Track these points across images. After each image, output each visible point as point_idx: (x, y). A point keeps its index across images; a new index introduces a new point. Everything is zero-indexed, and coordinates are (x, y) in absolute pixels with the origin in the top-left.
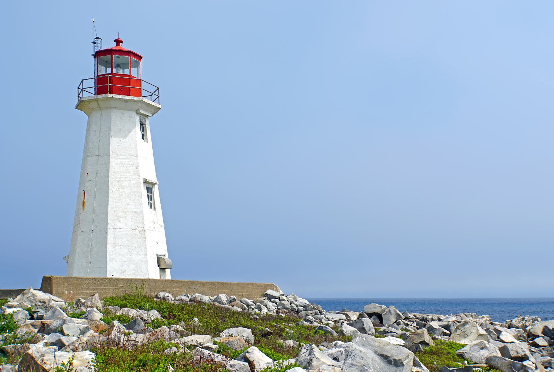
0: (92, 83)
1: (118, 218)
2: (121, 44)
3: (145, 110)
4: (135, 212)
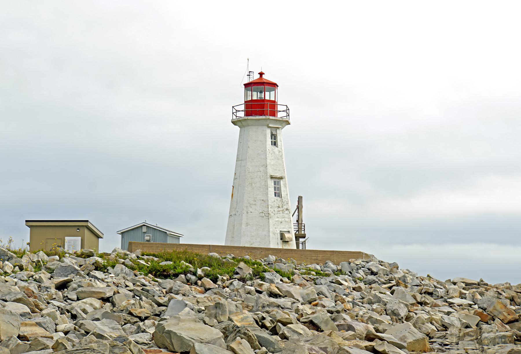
0: (243, 108)
2: (263, 75)
4: (263, 200)
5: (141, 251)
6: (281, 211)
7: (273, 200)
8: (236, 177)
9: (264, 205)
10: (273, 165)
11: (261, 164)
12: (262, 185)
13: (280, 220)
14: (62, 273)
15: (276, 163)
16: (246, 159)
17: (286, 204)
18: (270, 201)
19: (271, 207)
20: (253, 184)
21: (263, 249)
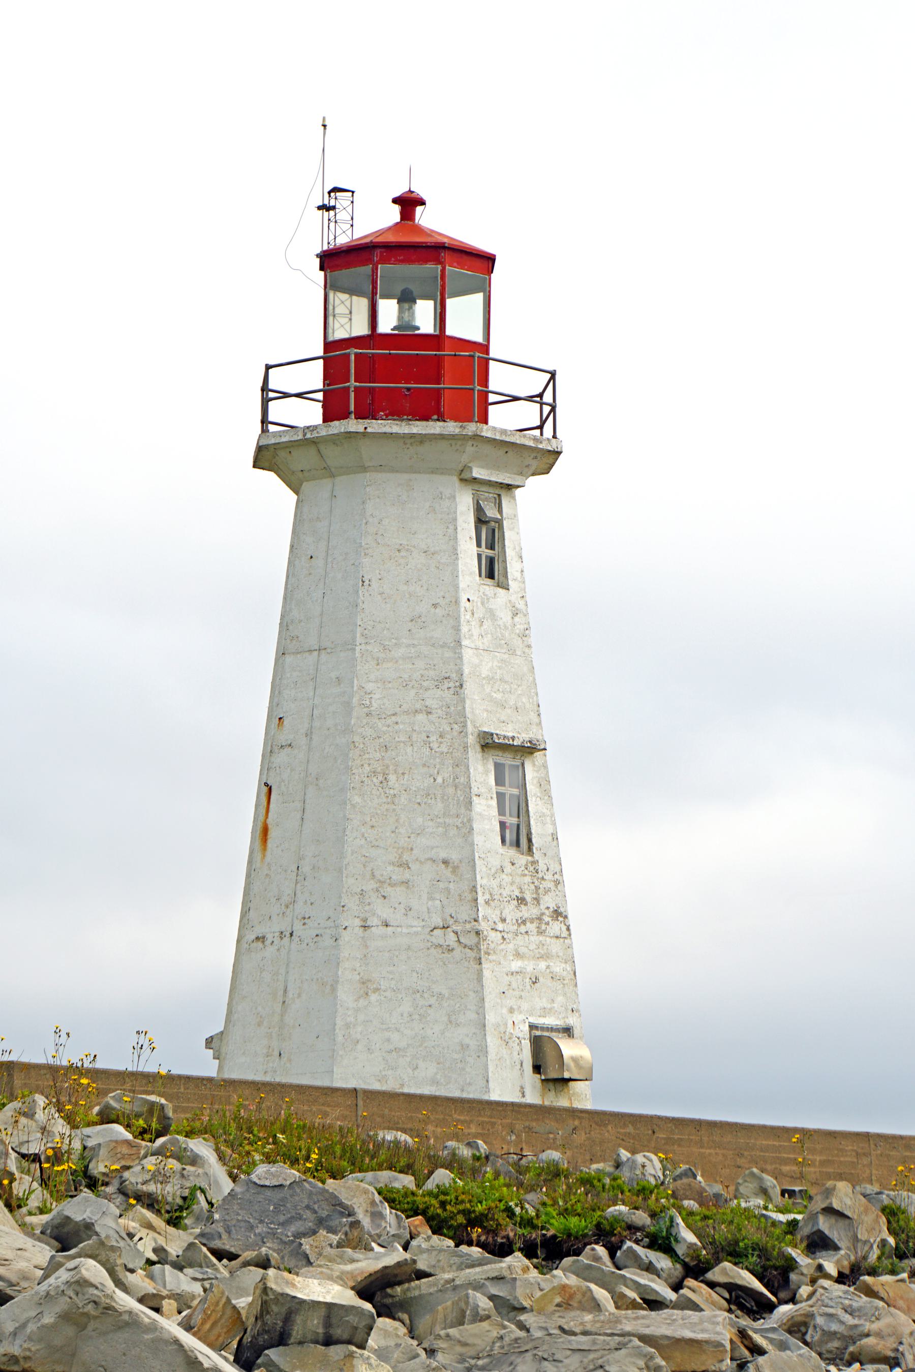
1: (378, 885)
2: (419, 209)
3: (496, 466)
4: (445, 862)
5: (579, 1101)
6: (532, 922)
7: (495, 862)
8: (284, 737)
9: (452, 886)
10: (490, 679)
11: (432, 673)
12: (439, 780)
13: (529, 966)
14: (261, 1229)
15: (500, 668)
16: (350, 646)
17: (551, 885)
18: (484, 869)
19: (487, 896)
20: (392, 778)
21: (579, 1118)
